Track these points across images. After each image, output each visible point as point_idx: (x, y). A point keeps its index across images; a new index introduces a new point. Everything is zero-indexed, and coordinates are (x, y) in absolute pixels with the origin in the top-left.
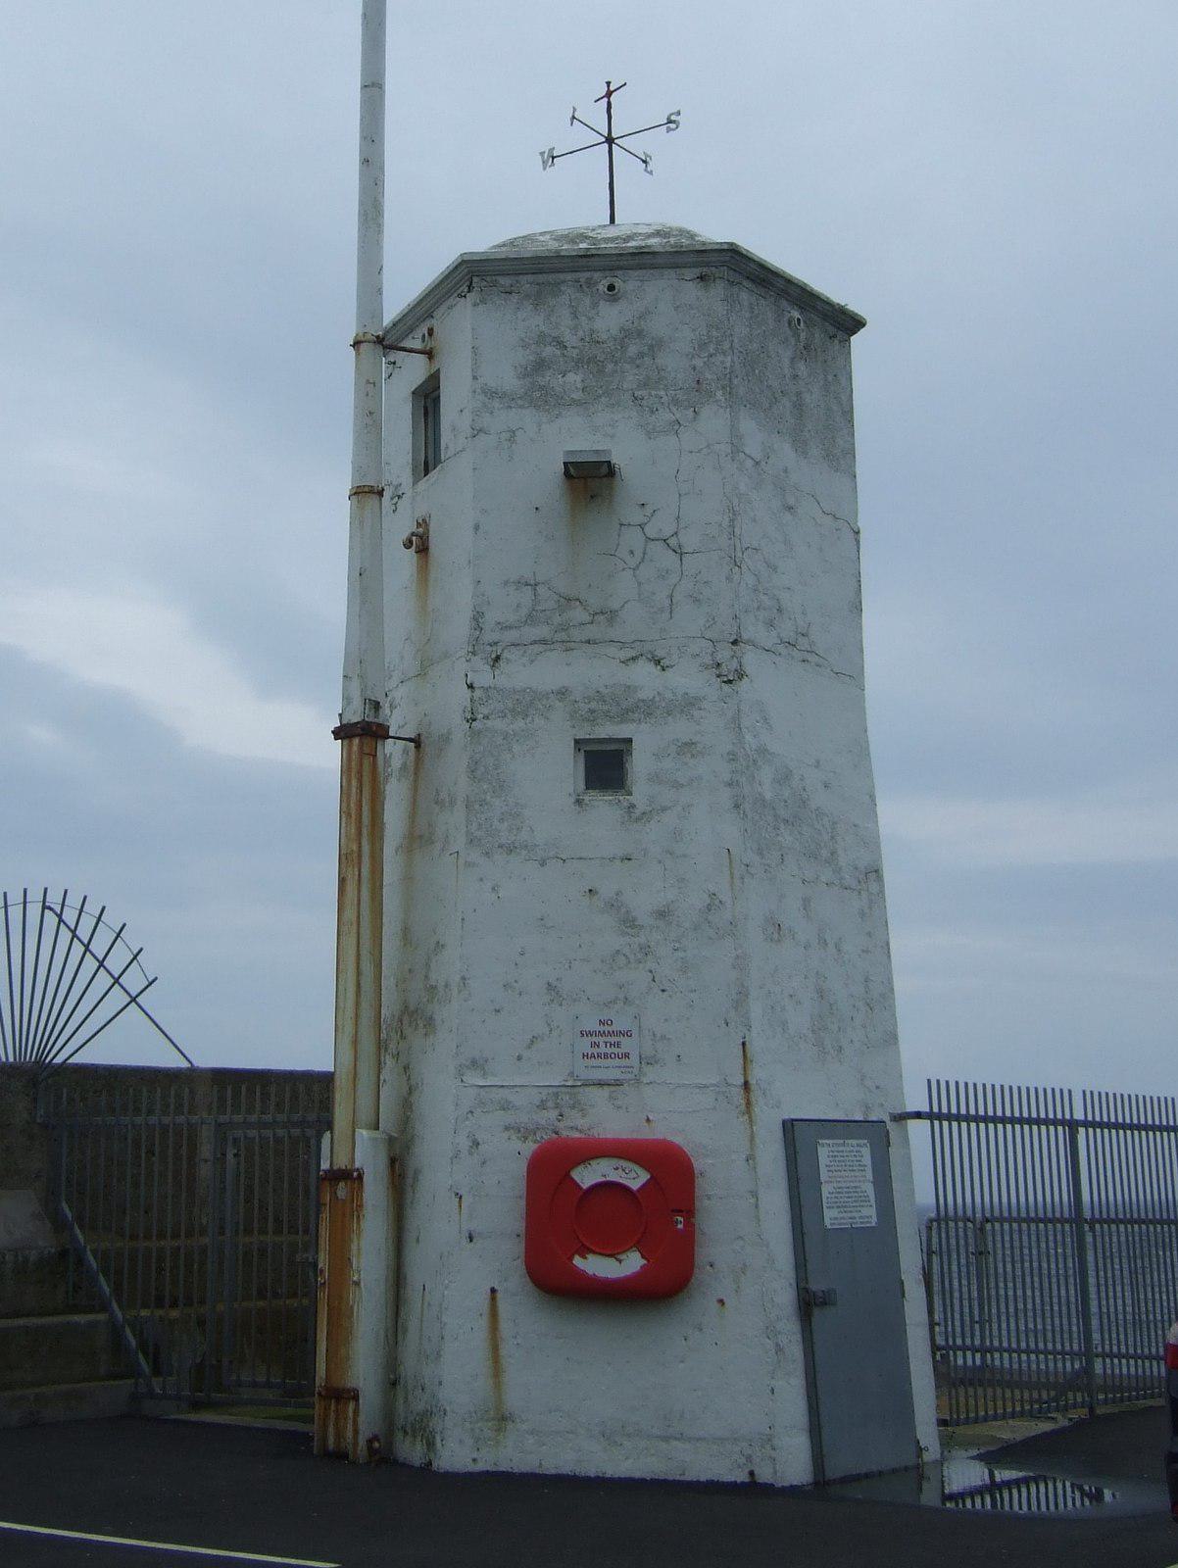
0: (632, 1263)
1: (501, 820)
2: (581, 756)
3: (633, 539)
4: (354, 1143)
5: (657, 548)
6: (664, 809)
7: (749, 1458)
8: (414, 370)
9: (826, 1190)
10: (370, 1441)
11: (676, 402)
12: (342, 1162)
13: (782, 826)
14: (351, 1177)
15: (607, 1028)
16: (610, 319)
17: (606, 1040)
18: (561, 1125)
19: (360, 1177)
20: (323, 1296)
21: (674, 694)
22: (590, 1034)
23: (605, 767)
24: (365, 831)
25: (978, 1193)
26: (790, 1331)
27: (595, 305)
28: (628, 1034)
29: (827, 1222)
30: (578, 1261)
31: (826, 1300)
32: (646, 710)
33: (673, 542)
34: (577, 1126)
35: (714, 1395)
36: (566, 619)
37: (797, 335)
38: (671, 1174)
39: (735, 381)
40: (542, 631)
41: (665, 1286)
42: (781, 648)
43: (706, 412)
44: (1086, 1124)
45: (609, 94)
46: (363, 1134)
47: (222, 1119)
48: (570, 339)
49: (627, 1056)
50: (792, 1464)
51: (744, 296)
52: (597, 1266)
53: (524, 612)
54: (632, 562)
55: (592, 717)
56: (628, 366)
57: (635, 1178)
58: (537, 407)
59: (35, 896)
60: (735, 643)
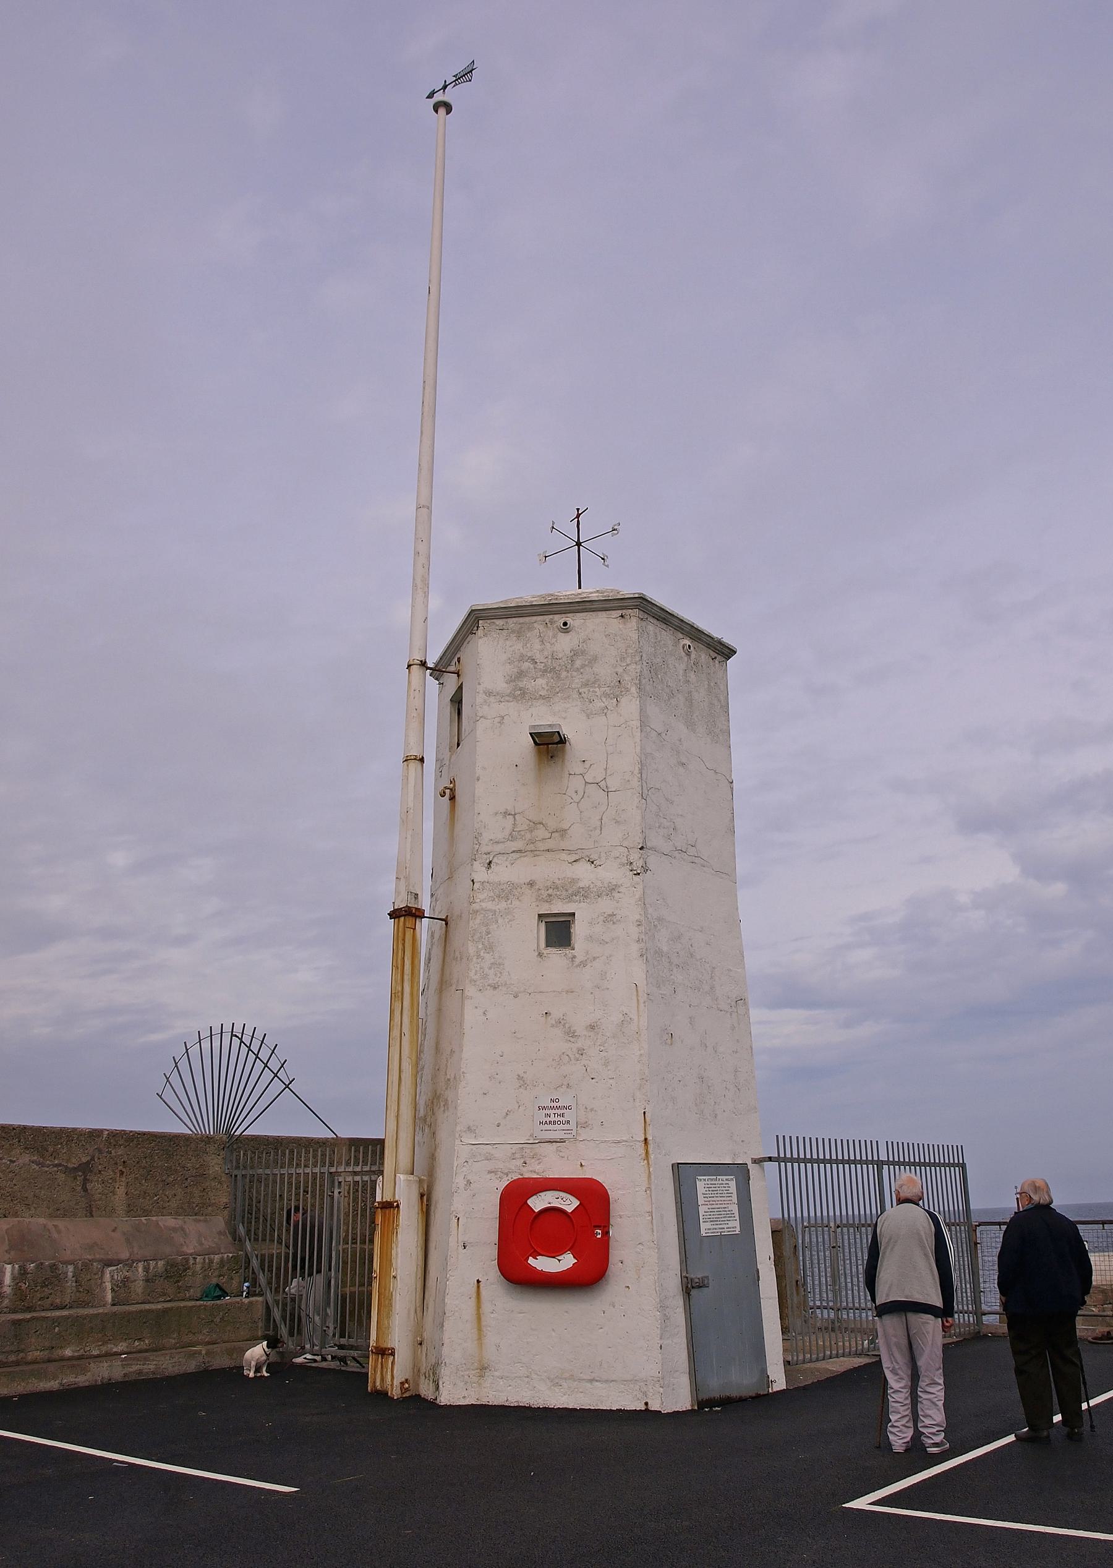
0: (567, 1261)
1: (490, 968)
2: (543, 926)
3: (576, 783)
4: (397, 1185)
5: (591, 789)
6: (595, 958)
7: (645, 1394)
8: (451, 682)
9: (702, 1210)
10: (402, 1384)
11: (606, 695)
12: (388, 1198)
13: (675, 970)
14: (390, 1206)
15: (555, 1104)
16: (565, 644)
17: (555, 1111)
18: (524, 1169)
19: (398, 1206)
20: (375, 1285)
21: (603, 883)
22: (544, 1108)
23: (559, 931)
24: (406, 977)
25: (805, 1210)
26: (679, 1302)
27: (555, 636)
28: (569, 1108)
29: (703, 1233)
30: (531, 1261)
31: (701, 1285)
32: (583, 894)
33: (602, 784)
34: (535, 1171)
35: (615, 1352)
36: (534, 837)
37: (688, 654)
38: (594, 1199)
39: (644, 681)
40: (518, 845)
41: (589, 1277)
42: (676, 854)
43: (624, 701)
44: (888, 1163)
45: (578, 516)
46: (401, 1177)
47: (333, 1170)
48: (539, 657)
49: (568, 1122)
50: (680, 1399)
51: (651, 628)
52: (544, 1264)
53: (507, 832)
54: (576, 798)
55: (549, 899)
56: (575, 674)
57: (569, 1204)
58: (517, 701)
59: (227, 1028)
60: (641, 848)
